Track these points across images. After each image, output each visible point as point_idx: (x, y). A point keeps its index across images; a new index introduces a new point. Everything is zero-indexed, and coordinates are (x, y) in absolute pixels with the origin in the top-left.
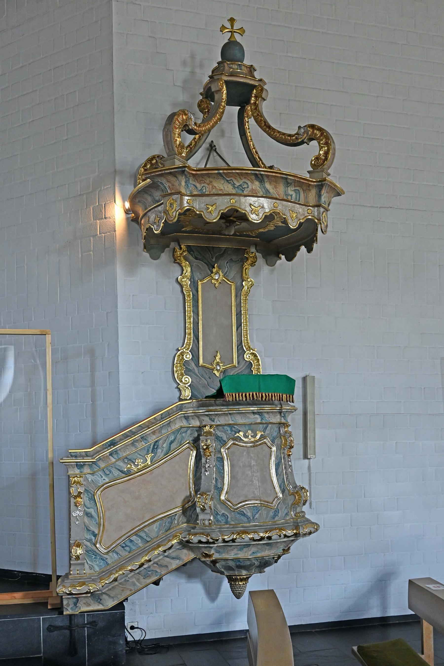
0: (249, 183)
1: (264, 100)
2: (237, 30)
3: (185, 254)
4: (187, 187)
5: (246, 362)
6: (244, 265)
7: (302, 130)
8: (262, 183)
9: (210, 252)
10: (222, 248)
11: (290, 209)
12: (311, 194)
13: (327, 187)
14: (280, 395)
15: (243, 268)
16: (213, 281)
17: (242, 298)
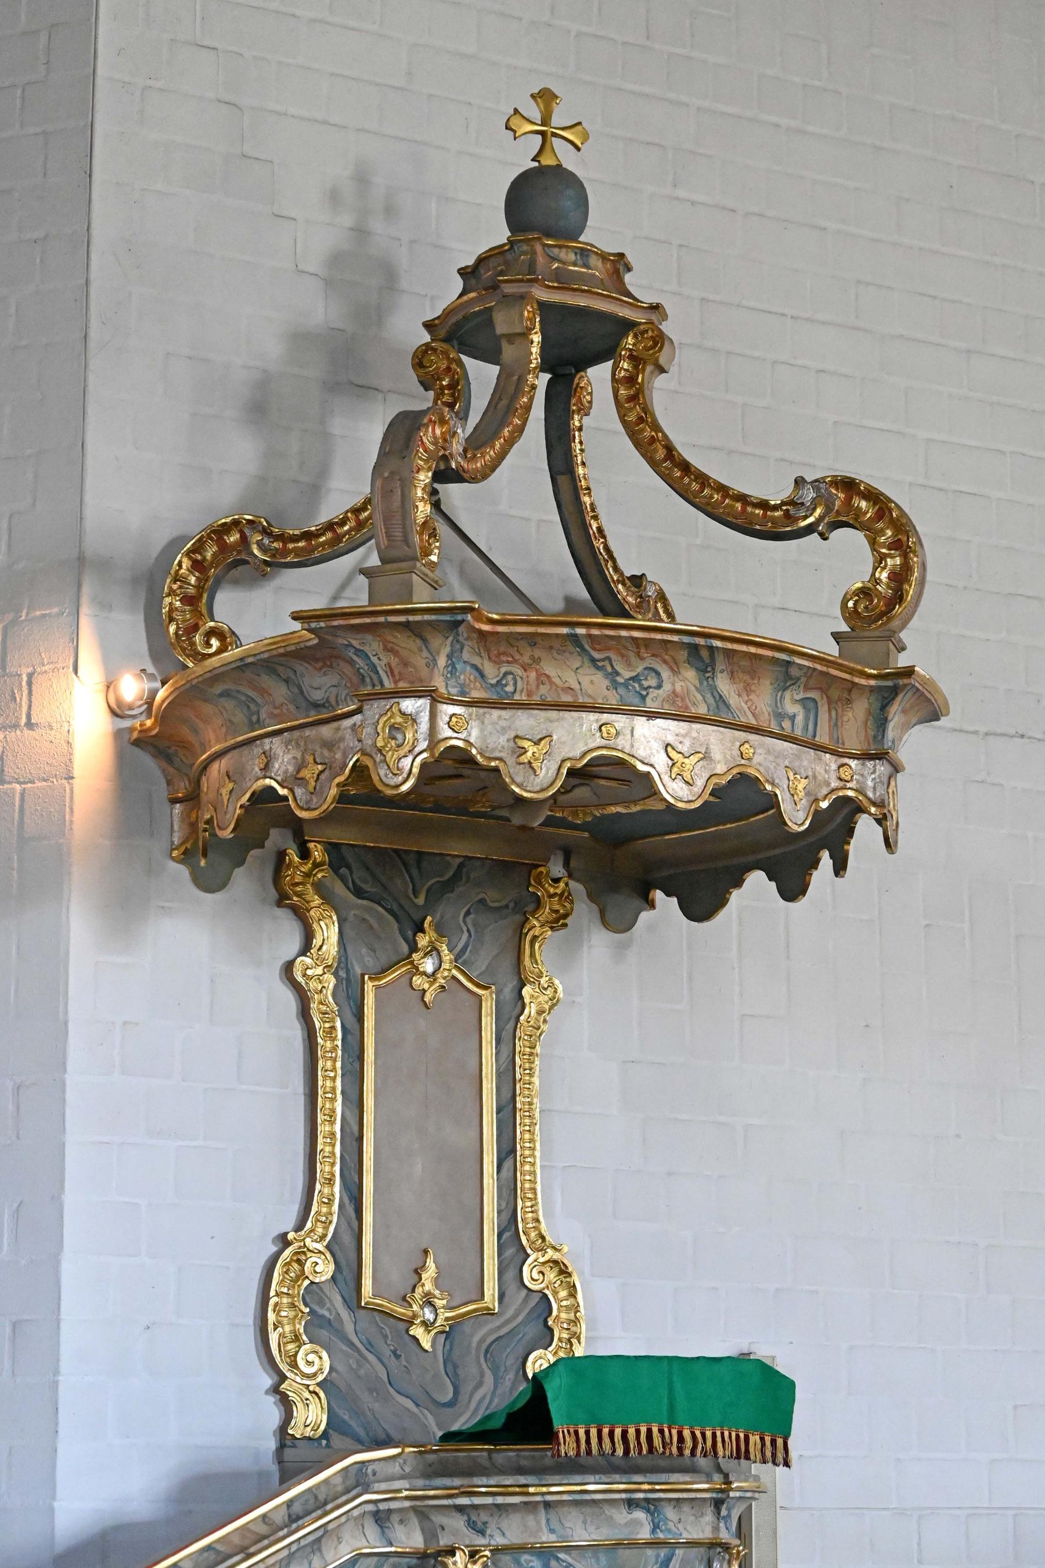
0: (665, 674)
1: (662, 370)
2: (563, 129)
3: (319, 876)
4: (451, 672)
5: (527, 1295)
6: (528, 926)
7: (809, 495)
8: (708, 675)
9: (407, 871)
10: (448, 858)
11: (787, 764)
12: (850, 714)
13: (910, 694)
14: (738, 1436)
15: (521, 937)
16: (417, 981)
17: (518, 1049)
